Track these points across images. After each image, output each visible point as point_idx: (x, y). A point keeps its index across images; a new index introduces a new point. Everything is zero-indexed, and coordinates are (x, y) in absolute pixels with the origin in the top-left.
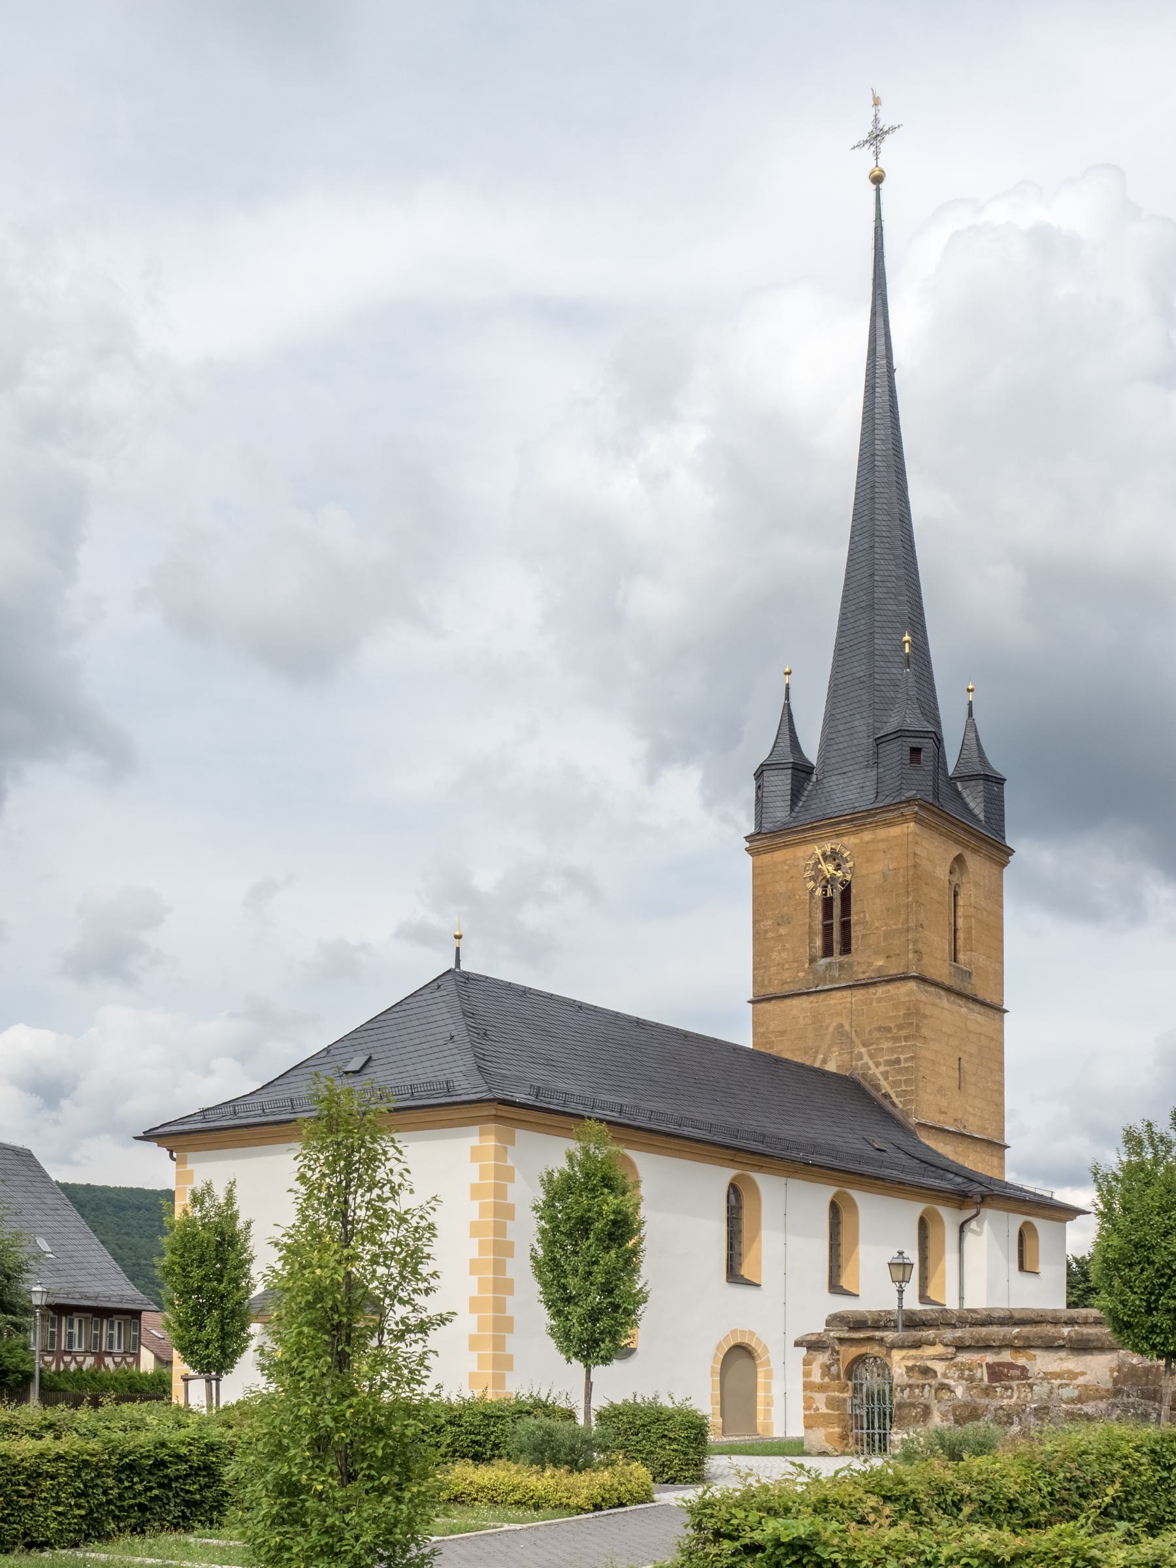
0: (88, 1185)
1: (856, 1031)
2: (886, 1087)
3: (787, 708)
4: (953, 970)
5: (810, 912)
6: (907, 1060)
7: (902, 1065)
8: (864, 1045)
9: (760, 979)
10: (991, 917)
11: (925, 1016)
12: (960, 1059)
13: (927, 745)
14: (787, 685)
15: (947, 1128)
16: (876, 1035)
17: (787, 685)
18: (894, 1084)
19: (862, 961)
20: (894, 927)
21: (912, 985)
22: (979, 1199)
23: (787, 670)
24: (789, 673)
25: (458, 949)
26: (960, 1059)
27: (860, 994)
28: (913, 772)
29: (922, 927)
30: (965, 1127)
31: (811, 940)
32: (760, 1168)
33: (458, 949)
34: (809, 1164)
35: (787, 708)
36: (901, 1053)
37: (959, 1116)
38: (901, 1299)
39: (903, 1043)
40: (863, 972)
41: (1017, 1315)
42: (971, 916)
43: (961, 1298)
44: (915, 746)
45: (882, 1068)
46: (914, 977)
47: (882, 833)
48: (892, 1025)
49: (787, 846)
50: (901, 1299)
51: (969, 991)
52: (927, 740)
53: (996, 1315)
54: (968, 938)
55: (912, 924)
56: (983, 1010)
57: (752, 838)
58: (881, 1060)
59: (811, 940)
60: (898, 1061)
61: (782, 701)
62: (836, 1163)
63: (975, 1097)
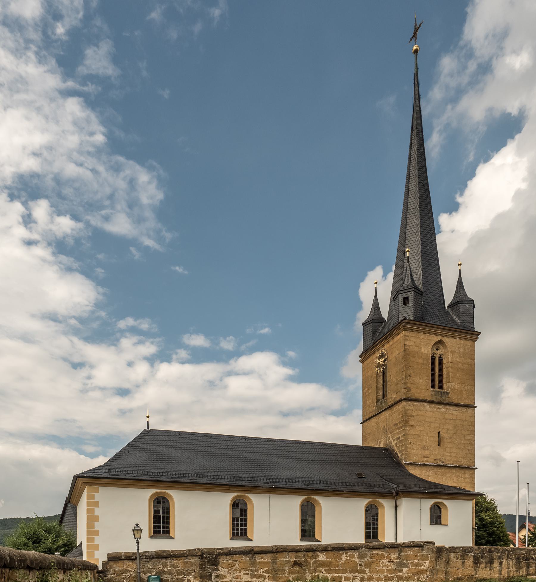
0: (522, 515)
1: (388, 428)
2: (397, 451)
3: (376, 297)
4: (434, 393)
5: (377, 381)
6: (402, 436)
7: (401, 439)
8: (391, 433)
9: (364, 413)
10: (465, 365)
11: (412, 416)
12: (439, 433)
13: (411, 295)
14: (376, 288)
15: (428, 464)
16: (394, 428)
17: (376, 288)
18: (399, 448)
19: (390, 397)
20: (399, 379)
21: (404, 403)
22: (395, 494)
23: (376, 282)
24: (376, 283)
25: (148, 422)
26: (439, 433)
27: (389, 411)
28: (404, 308)
29: (410, 376)
30: (443, 462)
31: (377, 393)
32: (250, 492)
33: (148, 422)
34: (273, 488)
35: (376, 297)
36: (400, 434)
37: (439, 457)
38: (138, 546)
39: (401, 429)
40: (390, 402)
41: (256, 550)
42: (449, 367)
43: (396, 539)
44: (405, 296)
45: (395, 442)
46: (405, 399)
47: (396, 339)
48: (398, 422)
49: (370, 356)
50: (138, 546)
51: (447, 400)
52: (411, 292)
53: (345, 546)
54: (448, 377)
55: (404, 376)
56: (457, 408)
57: (361, 356)
58: (395, 438)
59: (377, 393)
60: (399, 438)
61: (374, 295)
62: (304, 487)
63: (451, 448)
